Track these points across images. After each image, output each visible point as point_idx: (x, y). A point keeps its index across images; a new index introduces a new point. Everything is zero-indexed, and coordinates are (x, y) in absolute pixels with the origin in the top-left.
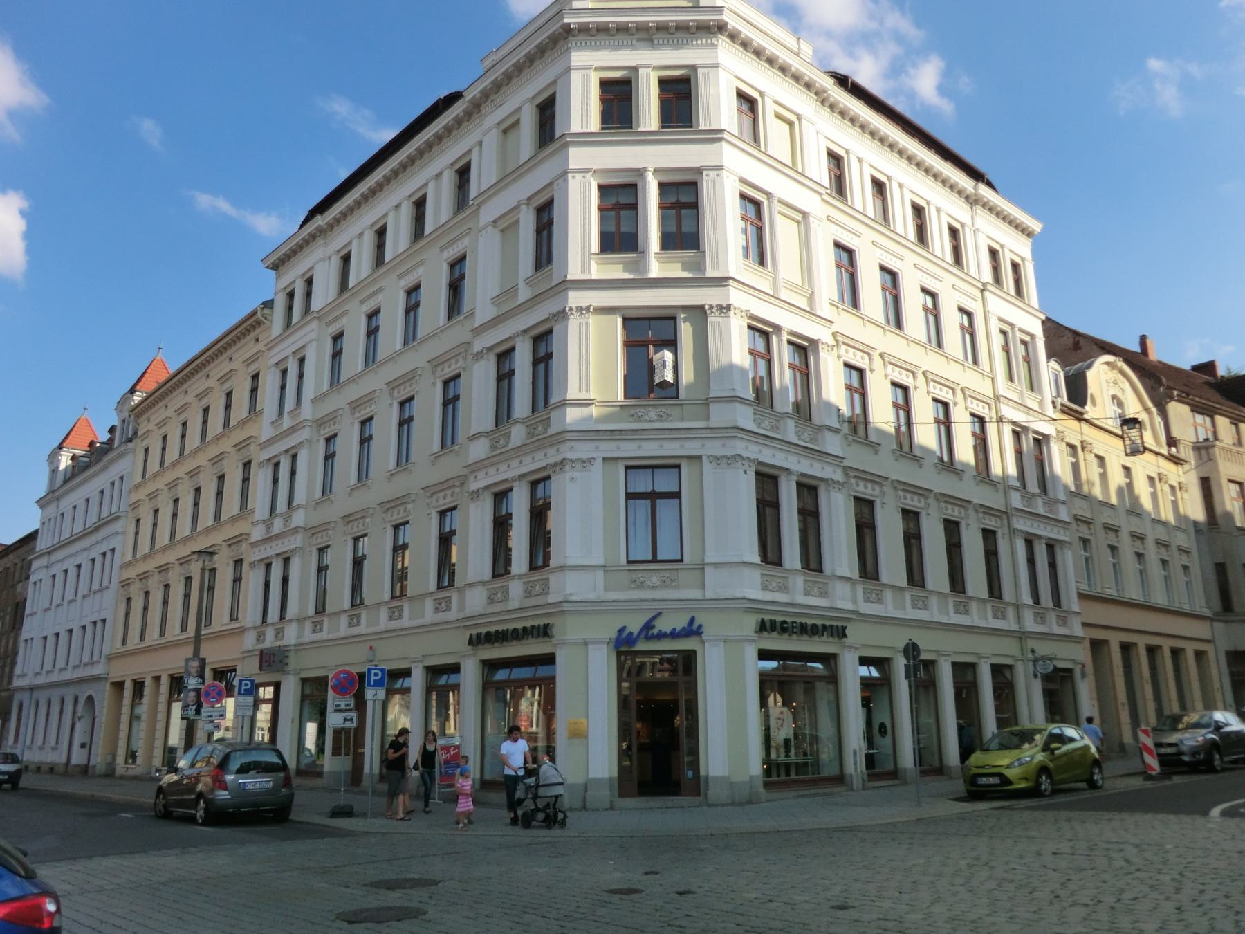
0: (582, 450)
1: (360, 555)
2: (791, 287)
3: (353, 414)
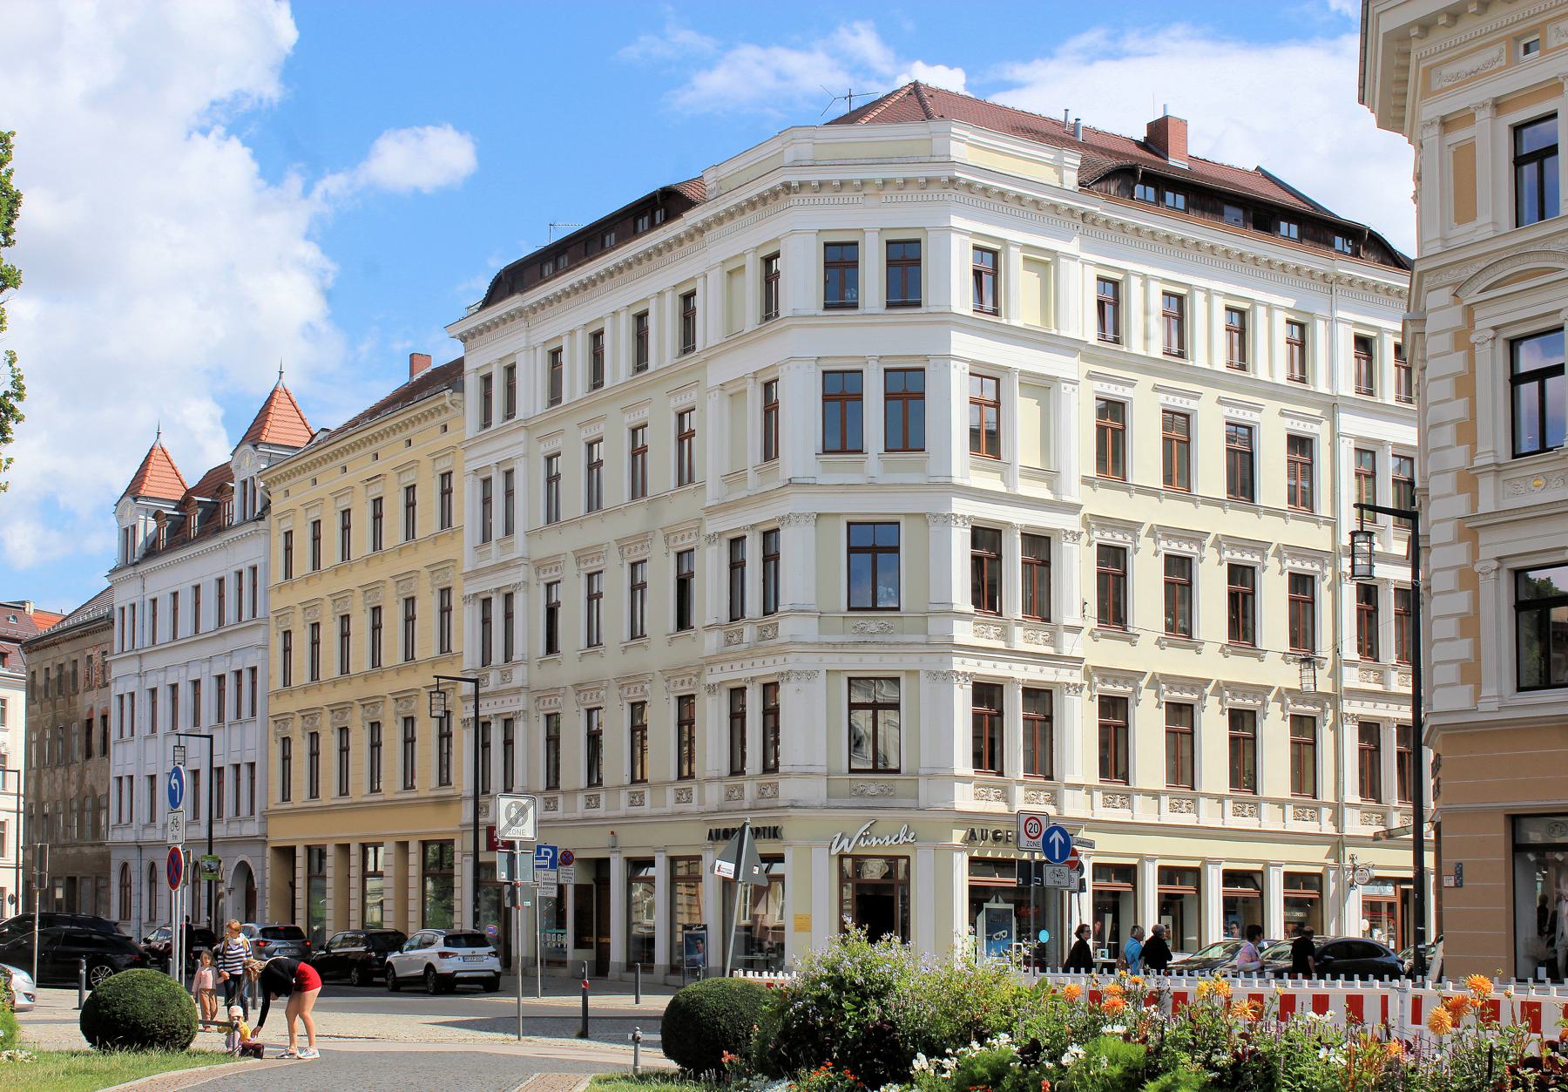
0: (809, 662)
1: (554, 601)
2: (1031, 473)
3: (578, 563)
